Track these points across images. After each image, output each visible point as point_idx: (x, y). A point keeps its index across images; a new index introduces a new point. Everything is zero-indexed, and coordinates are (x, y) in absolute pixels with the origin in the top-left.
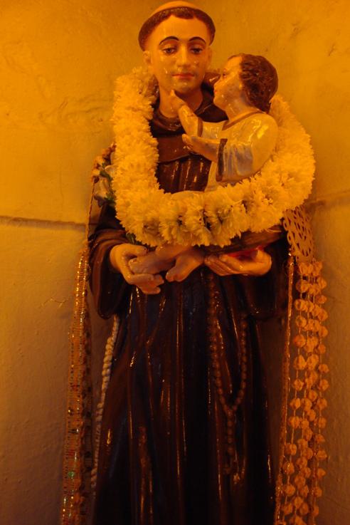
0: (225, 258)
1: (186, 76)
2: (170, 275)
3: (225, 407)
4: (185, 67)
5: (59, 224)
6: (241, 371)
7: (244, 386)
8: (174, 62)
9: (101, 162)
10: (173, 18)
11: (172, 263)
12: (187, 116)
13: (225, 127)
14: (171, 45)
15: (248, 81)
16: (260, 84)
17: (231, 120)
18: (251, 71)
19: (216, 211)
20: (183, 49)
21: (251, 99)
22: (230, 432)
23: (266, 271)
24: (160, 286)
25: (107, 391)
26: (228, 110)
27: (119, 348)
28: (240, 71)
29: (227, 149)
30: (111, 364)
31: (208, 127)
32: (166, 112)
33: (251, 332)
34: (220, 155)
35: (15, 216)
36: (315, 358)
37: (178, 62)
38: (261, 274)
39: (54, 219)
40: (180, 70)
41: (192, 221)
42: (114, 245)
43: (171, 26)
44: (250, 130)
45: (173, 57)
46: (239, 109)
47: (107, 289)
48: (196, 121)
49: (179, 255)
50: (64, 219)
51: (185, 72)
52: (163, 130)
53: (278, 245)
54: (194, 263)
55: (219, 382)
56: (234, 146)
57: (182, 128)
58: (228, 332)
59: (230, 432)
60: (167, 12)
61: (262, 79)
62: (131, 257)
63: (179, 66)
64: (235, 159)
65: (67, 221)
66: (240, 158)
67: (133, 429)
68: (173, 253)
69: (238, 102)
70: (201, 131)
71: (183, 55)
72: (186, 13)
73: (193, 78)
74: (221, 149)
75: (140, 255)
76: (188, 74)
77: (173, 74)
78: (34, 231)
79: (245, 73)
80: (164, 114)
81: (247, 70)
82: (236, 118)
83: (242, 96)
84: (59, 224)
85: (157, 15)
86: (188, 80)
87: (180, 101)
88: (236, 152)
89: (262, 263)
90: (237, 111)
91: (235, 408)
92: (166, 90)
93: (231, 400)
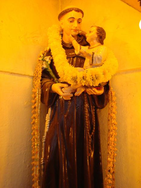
0: (94, 89)
1: (76, 30)
2: (76, 94)
3: (89, 135)
4: (76, 27)
5: (25, 75)
6: (93, 124)
7: (94, 128)
8: (72, 26)
9: (42, 55)
10: (73, 11)
11: (76, 91)
12: (75, 43)
13: (89, 48)
14: (72, 20)
15: (99, 35)
16: (101, 36)
17: (92, 46)
18: (100, 32)
19: (95, 75)
20: (76, 22)
21: (99, 40)
22: (90, 143)
23: (102, 93)
24: (71, 97)
25: (47, 133)
26: (91, 43)
27: (52, 118)
28: (97, 31)
29: (95, 55)
30: (49, 123)
31: (83, 47)
32: (66, 41)
33: (96, 112)
34: (93, 57)
35: (11, 72)
36: (33, 96)
37: (74, 26)
38: (100, 94)
39: (24, 74)
40: (74, 28)
41: (88, 78)
42: (52, 84)
43: (73, 14)
44: (99, 51)
45: (72, 24)
46: (95, 43)
47: (50, 99)
48: (79, 45)
49: (78, 88)
50: (27, 74)
51: (76, 29)
52: (68, 48)
53: (107, 86)
54: (83, 90)
55: (88, 127)
56: (97, 55)
57: (73, 46)
58: (90, 113)
59: (90, 143)
60: (72, 9)
61: (103, 35)
62: (62, 88)
63: (74, 27)
64: (97, 59)
65: (27, 74)
66: (98, 59)
67: (76, 154)
68: (77, 87)
69: (95, 41)
70: (81, 48)
71: (75, 24)
72: (78, 10)
73: (77, 31)
74: (93, 55)
75: (66, 87)
76: (76, 30)
77: (72, 29)
78: (17, 77)
79: (98, 32)
80: (65, 41)
81: (99, 31)
82: (94, 46)
83: (96, 39)
84: (25, 75)
85: (68, 9)
86: (76, 32)
87: (73, 38)
88: (97, 56)
89: (101, 92)
90: (94, 44)
91: (91, 136)
92: (67, 34)
93: (90, 134)
